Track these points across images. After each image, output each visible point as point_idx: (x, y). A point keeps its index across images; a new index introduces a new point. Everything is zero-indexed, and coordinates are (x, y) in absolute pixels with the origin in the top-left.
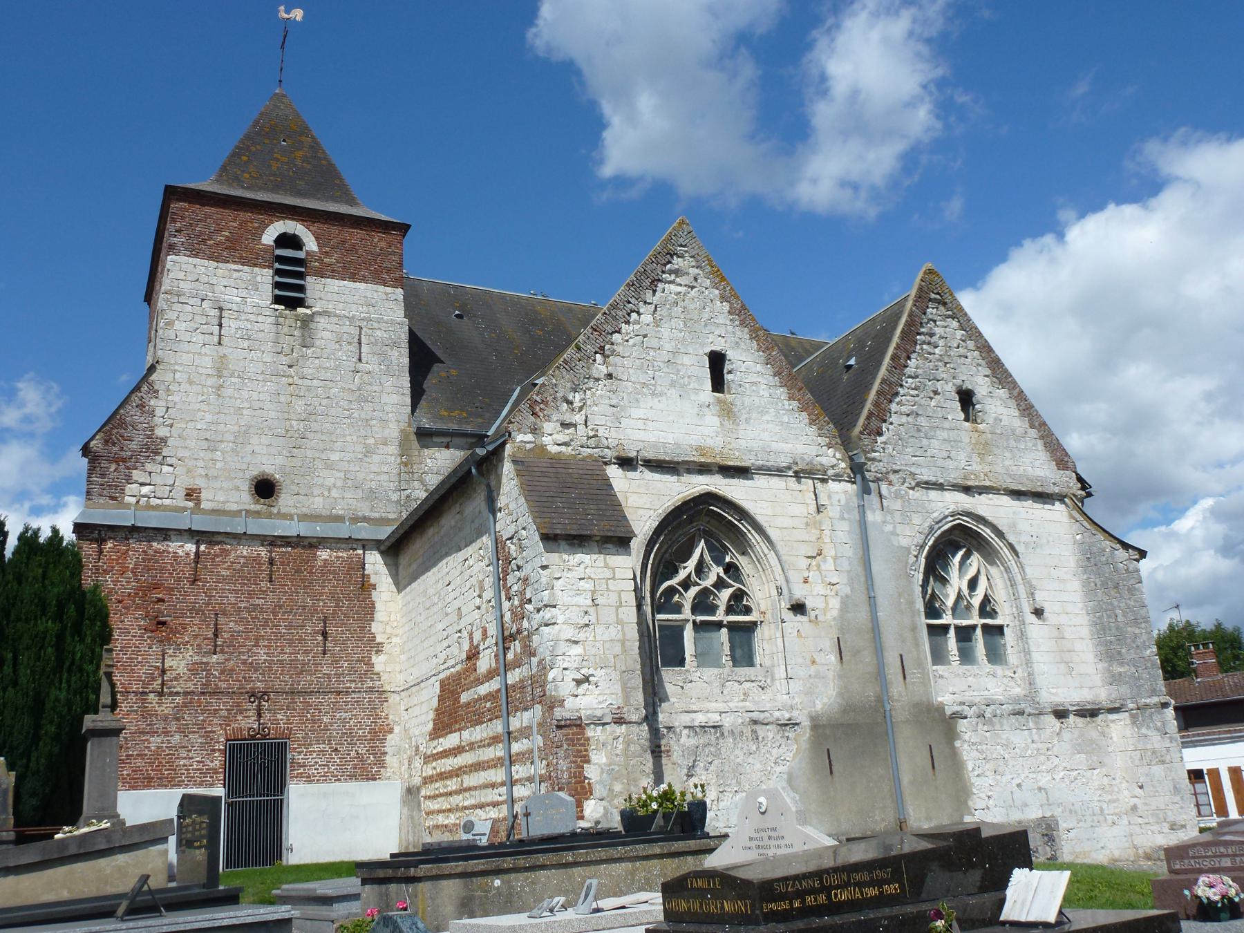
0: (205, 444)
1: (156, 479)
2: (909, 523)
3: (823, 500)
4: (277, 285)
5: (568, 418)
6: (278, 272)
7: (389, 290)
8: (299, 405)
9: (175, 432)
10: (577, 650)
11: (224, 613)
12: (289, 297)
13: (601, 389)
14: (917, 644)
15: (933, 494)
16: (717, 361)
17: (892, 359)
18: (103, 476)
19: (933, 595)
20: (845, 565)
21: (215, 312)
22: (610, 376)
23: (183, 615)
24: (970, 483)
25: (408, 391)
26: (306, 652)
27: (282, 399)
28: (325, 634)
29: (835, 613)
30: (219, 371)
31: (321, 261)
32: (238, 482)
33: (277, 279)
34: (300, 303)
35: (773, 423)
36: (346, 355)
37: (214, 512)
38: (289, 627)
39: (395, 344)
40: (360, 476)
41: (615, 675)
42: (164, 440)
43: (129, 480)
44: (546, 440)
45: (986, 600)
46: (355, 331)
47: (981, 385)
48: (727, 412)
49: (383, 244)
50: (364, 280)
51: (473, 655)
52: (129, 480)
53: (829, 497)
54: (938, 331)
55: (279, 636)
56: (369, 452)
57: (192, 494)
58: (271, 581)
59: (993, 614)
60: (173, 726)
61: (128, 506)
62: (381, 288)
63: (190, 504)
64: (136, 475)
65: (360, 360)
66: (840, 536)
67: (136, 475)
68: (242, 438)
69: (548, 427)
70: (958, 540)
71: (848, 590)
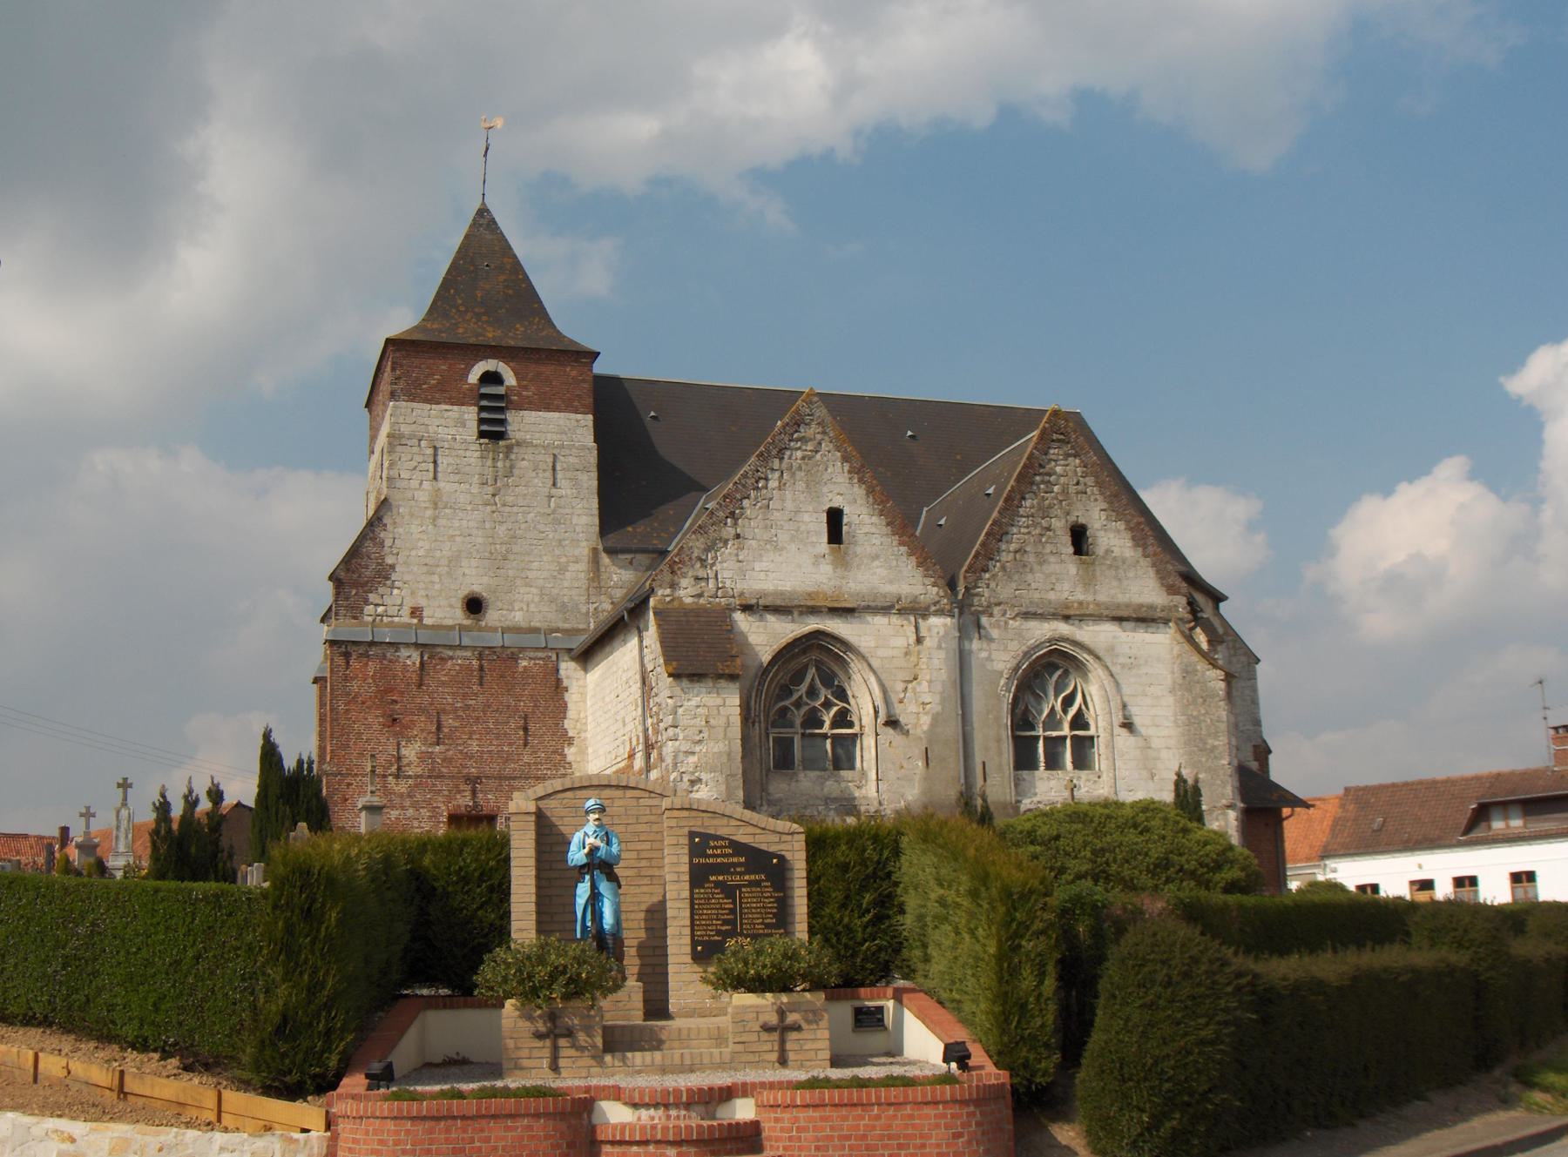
0: (425, 569)
1: (387, 600)
2: (1002, 653)
3: (923, 633)
4: (481, 421)
5: (701, 573)
6: (482, 409)
7: (579, 416)
8: (501, 530)
9: (401, 559)
10: (692, 759)
11: (444, 711)
12: (493, 433)
13: (730, 548)
14: (1000, 754)
15: (1033, 624)
16: (835, 518)
17: (1006, 501)
18: (347, 599)
19: (1027, 710)
20: (939, 688)
21: (430, 451)
22: (738, 536)
23: (413, 714)
24: (1071, 612)
25: (596, 512)
26: (510, 744)
27: (487, 525)
28: (526, 729)
29: (925, 728)
30: (436, 504)
31: (519, 394)
32: (453, 600)
33: (485, 415)
34: (500, 436)
35: (882, 565)
36: (541, 482)
37: (433, 627)
38: (496, 723)
39: (585, 470)
40: (555, 591)
41: (721, 779)
42: (392, 567)
43: (367, 602)
44: (681, 593)
45: (1079, 714)
46: (550, 460)
47: (1095, 515)
48: (842, 562)
49: (574, 373)
50: (558, 409)
51: (631, 756)
52: (367, 602)
53: (929, 629)
54: (1058, 469)
55: (488, 731)
56: (563, 570)
57: (416, 612)
58: (481, 684)
59: (1086, 726)
60: (407, 803)
61: (366, 624)
62: (573, 416)
63: (415, 621)
64: (372, 597)
65: (554, 484)
66: (936, 664)
67: (372, 597)
68: (454, 560)
69: (684, 582)
70: (1049, 668)
71: (939, 708)
